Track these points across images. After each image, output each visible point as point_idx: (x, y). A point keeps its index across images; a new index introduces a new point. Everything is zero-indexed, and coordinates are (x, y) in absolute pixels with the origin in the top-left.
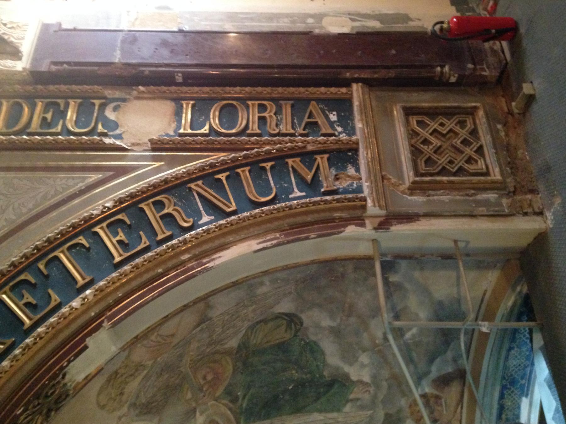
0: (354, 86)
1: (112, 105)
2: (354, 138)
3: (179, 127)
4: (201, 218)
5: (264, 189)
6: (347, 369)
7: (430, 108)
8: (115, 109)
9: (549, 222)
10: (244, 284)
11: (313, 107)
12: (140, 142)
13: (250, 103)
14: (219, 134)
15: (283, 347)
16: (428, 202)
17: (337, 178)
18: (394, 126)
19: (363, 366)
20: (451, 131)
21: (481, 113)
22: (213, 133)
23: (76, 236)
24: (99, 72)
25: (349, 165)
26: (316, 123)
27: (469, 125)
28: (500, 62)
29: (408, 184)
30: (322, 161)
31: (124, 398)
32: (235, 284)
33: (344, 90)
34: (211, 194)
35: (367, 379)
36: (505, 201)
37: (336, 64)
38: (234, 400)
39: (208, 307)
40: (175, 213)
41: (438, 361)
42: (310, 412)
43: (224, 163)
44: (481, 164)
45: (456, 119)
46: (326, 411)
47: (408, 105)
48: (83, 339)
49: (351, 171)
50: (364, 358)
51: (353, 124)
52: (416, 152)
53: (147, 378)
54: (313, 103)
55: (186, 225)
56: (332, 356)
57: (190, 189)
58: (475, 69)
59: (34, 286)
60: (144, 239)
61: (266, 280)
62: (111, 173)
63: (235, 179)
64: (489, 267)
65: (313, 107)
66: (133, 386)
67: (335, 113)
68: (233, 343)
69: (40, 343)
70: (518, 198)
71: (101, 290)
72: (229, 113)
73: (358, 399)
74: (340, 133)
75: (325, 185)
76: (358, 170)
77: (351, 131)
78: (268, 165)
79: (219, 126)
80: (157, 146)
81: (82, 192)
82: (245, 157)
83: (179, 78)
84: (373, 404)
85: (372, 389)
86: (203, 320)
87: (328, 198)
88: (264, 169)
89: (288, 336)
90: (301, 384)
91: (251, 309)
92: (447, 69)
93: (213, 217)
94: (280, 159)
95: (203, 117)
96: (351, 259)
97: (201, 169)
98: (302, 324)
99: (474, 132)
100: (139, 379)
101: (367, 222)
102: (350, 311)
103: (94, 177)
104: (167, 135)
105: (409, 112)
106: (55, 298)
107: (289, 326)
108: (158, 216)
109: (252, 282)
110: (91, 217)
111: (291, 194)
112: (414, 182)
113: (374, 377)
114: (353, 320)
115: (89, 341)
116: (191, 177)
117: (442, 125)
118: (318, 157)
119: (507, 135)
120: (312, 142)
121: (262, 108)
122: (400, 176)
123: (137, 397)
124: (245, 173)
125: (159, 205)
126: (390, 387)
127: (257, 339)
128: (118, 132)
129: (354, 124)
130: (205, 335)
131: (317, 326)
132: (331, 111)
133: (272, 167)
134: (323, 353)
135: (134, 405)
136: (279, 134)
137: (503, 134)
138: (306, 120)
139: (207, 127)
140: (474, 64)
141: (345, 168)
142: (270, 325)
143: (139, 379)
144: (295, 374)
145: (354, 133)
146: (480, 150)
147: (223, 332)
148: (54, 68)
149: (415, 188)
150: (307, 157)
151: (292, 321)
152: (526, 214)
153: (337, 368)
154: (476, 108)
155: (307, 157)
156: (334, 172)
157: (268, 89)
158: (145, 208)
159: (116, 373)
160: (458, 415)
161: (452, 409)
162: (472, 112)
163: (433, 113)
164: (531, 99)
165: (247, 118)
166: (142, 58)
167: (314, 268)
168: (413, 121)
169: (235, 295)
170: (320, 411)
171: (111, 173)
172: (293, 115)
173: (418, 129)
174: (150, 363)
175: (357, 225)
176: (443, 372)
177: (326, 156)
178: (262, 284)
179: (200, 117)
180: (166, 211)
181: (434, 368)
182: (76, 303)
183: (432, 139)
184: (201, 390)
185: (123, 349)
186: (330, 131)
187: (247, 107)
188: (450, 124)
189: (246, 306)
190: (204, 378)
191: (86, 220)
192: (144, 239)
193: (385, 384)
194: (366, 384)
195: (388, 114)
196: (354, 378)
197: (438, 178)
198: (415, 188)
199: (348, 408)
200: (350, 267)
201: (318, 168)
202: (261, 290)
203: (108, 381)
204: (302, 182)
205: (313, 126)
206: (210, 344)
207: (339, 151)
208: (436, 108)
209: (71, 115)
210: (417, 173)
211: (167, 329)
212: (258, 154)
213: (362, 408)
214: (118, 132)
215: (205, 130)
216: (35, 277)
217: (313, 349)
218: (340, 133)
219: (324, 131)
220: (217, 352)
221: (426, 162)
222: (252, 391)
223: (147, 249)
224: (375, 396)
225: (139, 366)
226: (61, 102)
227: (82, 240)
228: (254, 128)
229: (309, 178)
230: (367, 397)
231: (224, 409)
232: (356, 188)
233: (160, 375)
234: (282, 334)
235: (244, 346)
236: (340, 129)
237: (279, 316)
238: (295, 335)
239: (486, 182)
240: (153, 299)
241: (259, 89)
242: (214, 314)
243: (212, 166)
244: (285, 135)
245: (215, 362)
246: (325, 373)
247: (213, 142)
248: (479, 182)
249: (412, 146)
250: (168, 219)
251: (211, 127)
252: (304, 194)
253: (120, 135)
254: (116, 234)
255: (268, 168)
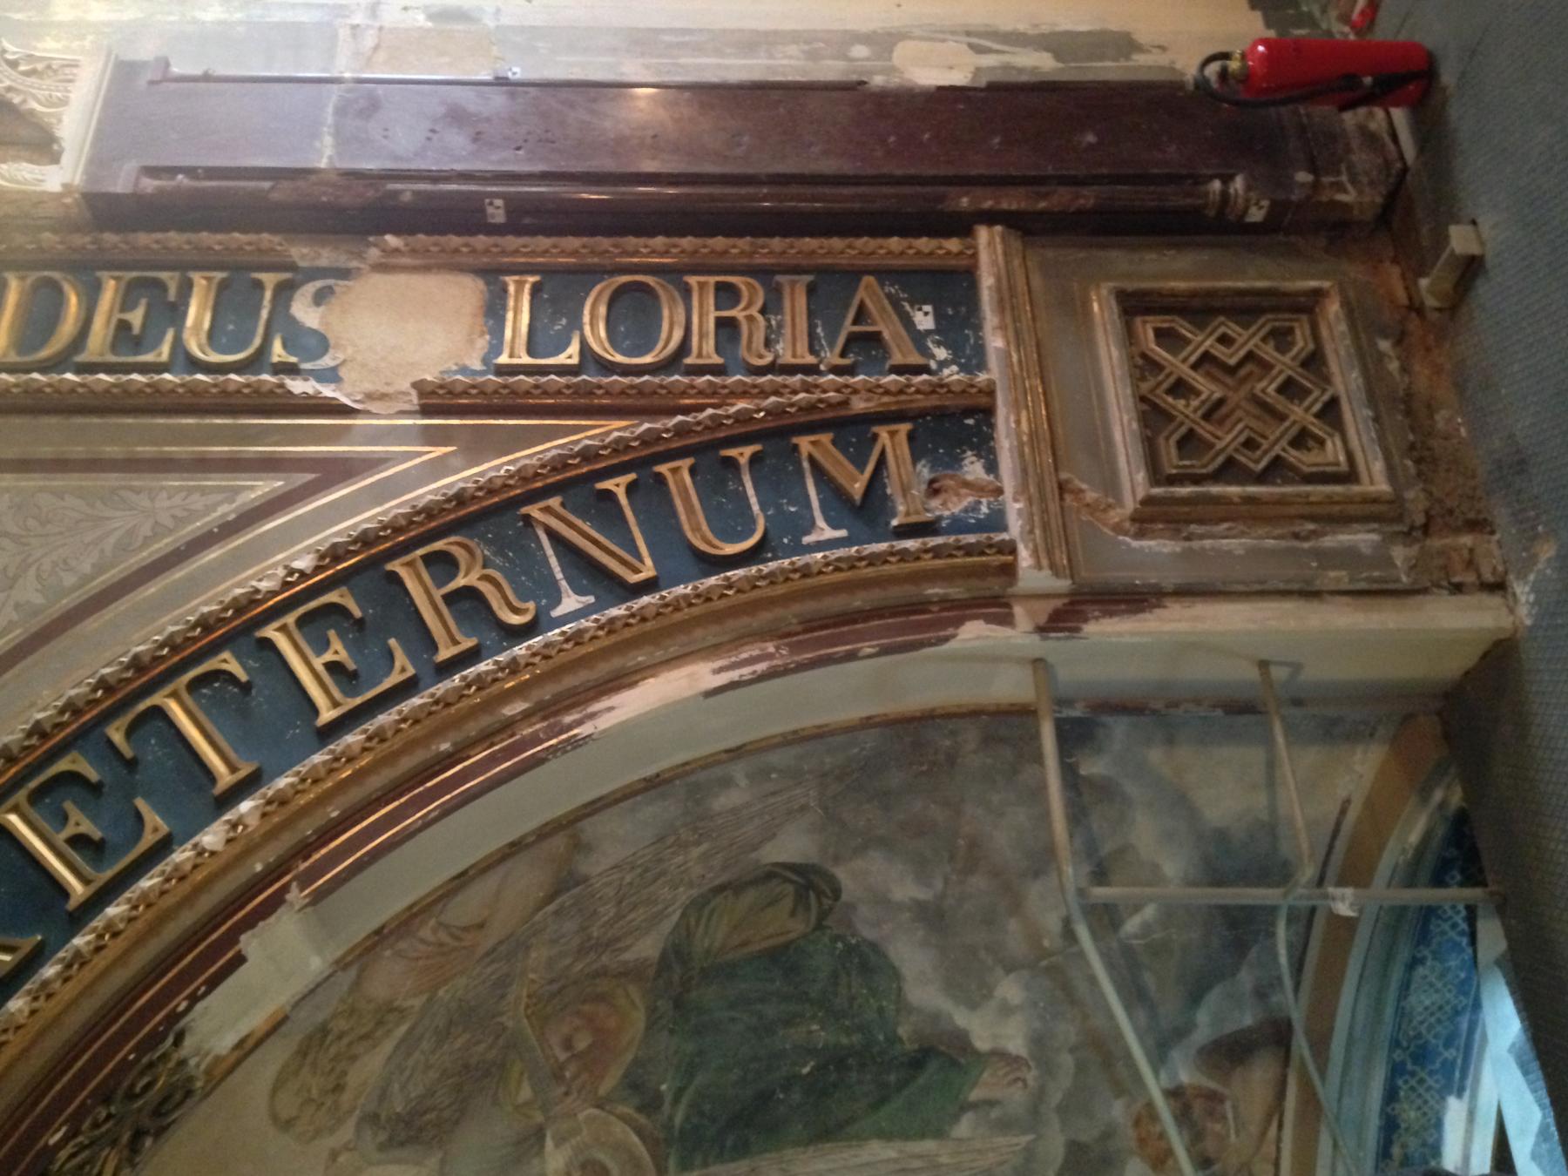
0: (983, 234)
1: (310, 288)
2: (982, 377)
3: (496, 349)
4: (557, 600)
5: (732, 520)
6: (962, 1018)
7: (1194, 294)
8: (320, 298)
9: (1523, 611)
10: (680, 787)
11: (868, 291)
12: (390, 390)
13: (693, 280)
14: (608, 368)
15: (782, 959)
16: (1188, 555)
17: (934, 490)
18: (1090, 343)
19: (1006, 1010)
20: (1250, 356)
21: (1333, 308)
22: (592, 366)
23: (213, 649)
24: (275, 196)
25: (969, 453)
26: (875, 339)
27: (1302, 342)
28: (1387, 164)
29: (1130, 505)
30: (892, 441)
31: (346, 1097)
32: (653, 784)
33: (953, 245)
34: (584, 534)
35: (1016, 1045)
36: (1400, 554)
37: (932, 172)
38: (651, 1105)
39: (579, 846)
40: (485, 588)
41: (1214, 997)
42: (861, 1138)
43: (620, 446)
44: (1334, 451)
45: (1266, 323)
46: (906, 1136)
47: (1131, 286)
48: (232, 938)
49: (973, 469)
50: (1010, 989)
51: (979, 338)
52: (1152, 416)
53: (408, 1044)
54: (869, 279)
55: (515, 620)
56: (922, 984)
57: (527, 518)
58: (1316, 186)
59: (96, 789)
60: (401, 659)
61: (739, 771)
62: (310, 477)
63: (650, 491)
64: (1357, 734)
65: (868, 291)
66: (371, 1066)
67: (928, 308)
68: (648, 948)
69: (115, 948)
70: (1436, 543)
71: (281, 800)
72: (634, 309)
73: (991, 1103)
74: (943, 364)
75: (901, 508)
76: (992, 467)
77: (973, 358)
78: (743, 454)
79: (607, 345)
80: (437, 400)
81: (228, 529)
82: (681, 431)
83: (497, 213)
84: (1034, 1117)
85: (1031, 1076)
86: (565, 882)
87: (911, 544)
88: (731, 463)
89: (797, 927)
90: (836, 1060)
91: (695, 852)
92: (1239, 184)
93: (591, 599)
94: (775, 436)
95: (564, 321)
96: (975, 713)
97: (559, 464)
98: (837, 893)
99: (1314, 361)
100: (388, 1047)
101: (1018, 610)
102: (972, 857)
103: (263, 487)
104: (464, 370)
105: (1133, 305)
106: (155, 823)
107: (801, 898)
108: (438, 594)
109: (701, 776)
110: (252, 599)
111: (808, 533)
112: (1148, 501)
113: (1039, 1042)
114: (978, 882)
115: (249, 943)
116: (531, 486)
117: (1225, 340)
118: (883, 433)
119: (1404, 369)
120: (866, 390)
121: (728, 295)
122: (1111, 485)
123: (383, 1095)
124: (679, 475)
125: (443, 564)
126: (1081, 1068)
127: (715, 936)
128: (327, 361)
129: (981, 338)
130: (570, 926)
131: (882, 901)
132: (917, 302)
133: (755, 459)
134: (896, 975)
135: (372, 1119)
136: (772, 368)
137: (1394, 366)
138: (848, 327)
139: (574, 348)
140: (1313, 169)
141: (956, 461)
142: (750, 896)
143: (388, 1047)
144: (820, 1034)
145: (982, 366)
146: (1331, 412)
147: (619, 916)
148: (149, 185)
149: (1149, 517)
150: (852, 430)
151: (810, 886)
152: (1458, 589)
153: (936, 1017)
154: (1318, 294)
155: (852, 430)
156: (925, 472)
157: (744, 243)
158: (403, 573)
159: (324, 1030)
160: (1269, 1149)
161: (1254, 1129)
162: (1308, 305)
163: (1200, 309)
164: (1472, 267)
165: (685, 322)
166: (397, 158)
167: (870, 740)
168: (1146, 330)
169: (653, 813)
170: (886, 1136)
171: (310, 477)
172: (811, 315)
173: (1161, 354)
174: (417, 1002)
175: (989, 619)
176: (1230, 1028)
177: (904, 428)
178: (727, 783)
179: (553, 321)
180: (460, 582)
181: (1203, 1017)
182: (212, 837)
183: (1198, 380)
184: (558, 1076)
185: (341, 964)
186: (915, 359)
187: (686, 292)
188: (1248, 339)
189: (683, 846)
190: (568, 1044)
191: (240, 606)
192: (401, 659)
193: (1067, 1061)
194: (1013, 1061)
195: (1077, 312)
196: (982, 1044)
197: (1215, 489)
198: (1149, 517)
199: (964, 1127)
200: (971, 736)
201: (882, 462)
202: (723, 801)
203: (303, 1052)
204: (838, 503)
205: (866, 345)
206: (582, 951)
207: (940, 414)
208: (1211, 293)
209: (197, 314)
210: (1156, 474)
211: (466, 908)
212: (717, 423)
213: (1005, 1126)
214: (327, 361)
215: (570, 355)
216: (95, 761)
217: (868, 962)
218: (943, 364)
219: (897, 358)
220: (602, 973)
221: (1181, 444)
222: (700, 1079)
223: (408, 688)
224: (1040, 1095)
225: (388, 1012)
226: (170, 278)
227: (228, 662)
228: (706, 350)
229: (857, 488)
230: (1016, 1098)
231: (620, 1130)
232: (988, 516)
233: (443, 1036)
234: (782, 923)
235: (676, 954)
236: (942, 353)
237: (772, 874)
238: (819, 926)
239: (1349, 500)
240: (427, 824)
241: (719, 242)
242: (595, 866)
243: (587, 455)
244: (791, 370)
245: (600, 998)
246: (903, 1031)
247: (589, 390)
248: (1330, 500)
249: (1143, 399)
250: (468, 603)
251: (585, 348)
252: (842, 533)
253: (334, 369)
254: (322, 646)
255: (743, 461)
